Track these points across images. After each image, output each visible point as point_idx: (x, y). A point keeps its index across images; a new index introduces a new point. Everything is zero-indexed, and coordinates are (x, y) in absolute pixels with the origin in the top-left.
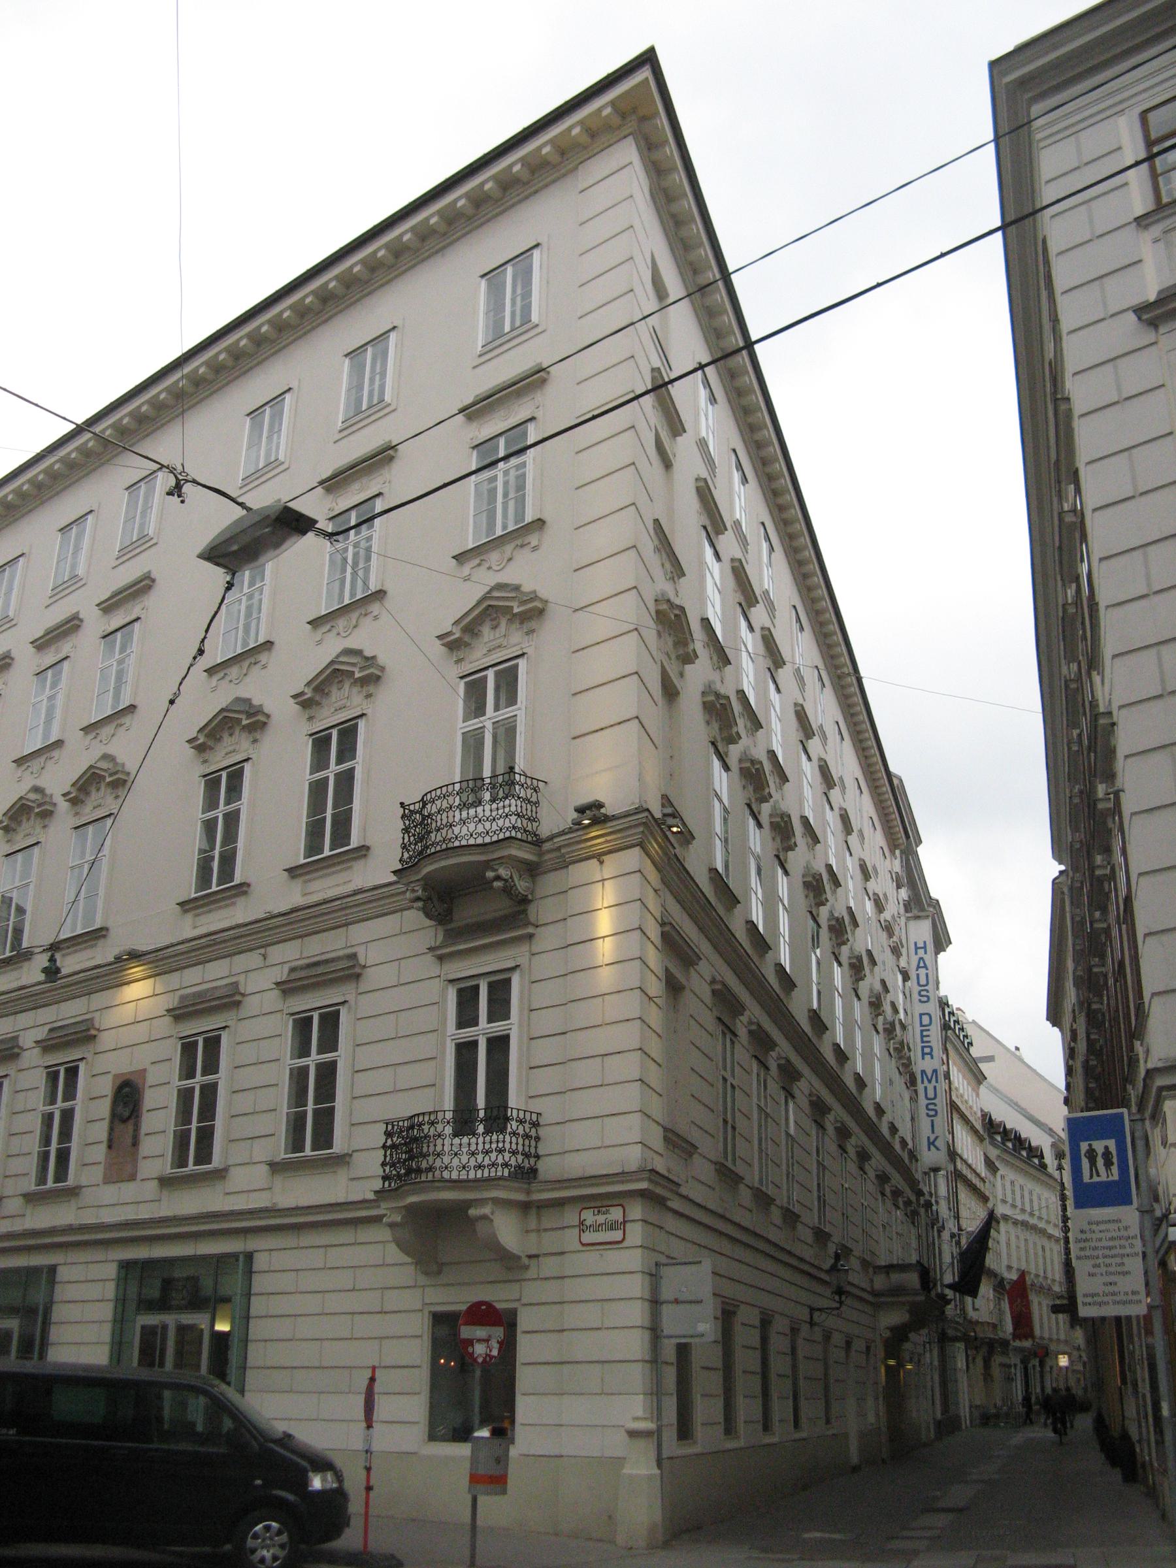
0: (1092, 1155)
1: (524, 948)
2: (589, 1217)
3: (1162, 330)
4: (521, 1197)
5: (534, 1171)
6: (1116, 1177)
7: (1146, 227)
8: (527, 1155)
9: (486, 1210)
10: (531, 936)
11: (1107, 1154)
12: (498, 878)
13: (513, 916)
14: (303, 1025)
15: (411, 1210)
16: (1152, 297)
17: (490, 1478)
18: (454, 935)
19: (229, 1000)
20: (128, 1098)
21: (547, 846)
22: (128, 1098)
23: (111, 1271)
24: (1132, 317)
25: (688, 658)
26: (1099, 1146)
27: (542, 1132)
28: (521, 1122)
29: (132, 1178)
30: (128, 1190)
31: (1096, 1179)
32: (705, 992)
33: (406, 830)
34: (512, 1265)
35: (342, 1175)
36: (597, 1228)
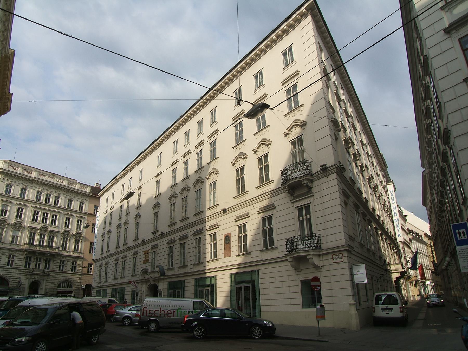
0: (459, 233)
1: (312, 198)
2: (334, 256)
3: (451, 33)
4: (318, 253)
5: (320, 247)
6: (467, 238)
7: (443, 9)
8: (318, 244)
9: (311, 256)
10: (313, 195)
11: (463, 232)
12: (304, 183)
13: (309, 191)
14: (239, 227)
15: (293, 258)
16: (447, 26)
17: (321, 316)
18: (295, 198)
19: (247, 216)
20: (227, 239)
21: (314, 175)
22: (227, 239)
23: (194, 280)
24: (443, 32)
25: (339, 130)
26: (461, 231)
27: (321, 238)
28: (316, 236)
29: (230, 256)
30: (229, 259)
31: (461, 239)
32: (352, 204)
33: (282, 176)
34: (317, 268)
35: (277, 251)
36: (337, 259)
